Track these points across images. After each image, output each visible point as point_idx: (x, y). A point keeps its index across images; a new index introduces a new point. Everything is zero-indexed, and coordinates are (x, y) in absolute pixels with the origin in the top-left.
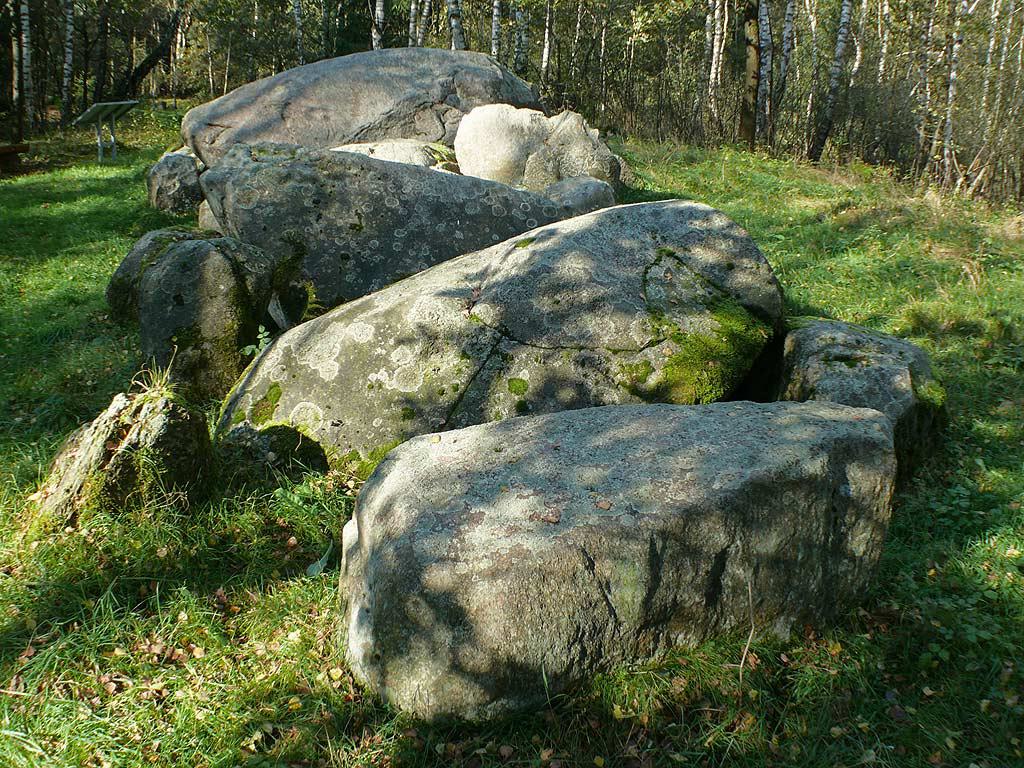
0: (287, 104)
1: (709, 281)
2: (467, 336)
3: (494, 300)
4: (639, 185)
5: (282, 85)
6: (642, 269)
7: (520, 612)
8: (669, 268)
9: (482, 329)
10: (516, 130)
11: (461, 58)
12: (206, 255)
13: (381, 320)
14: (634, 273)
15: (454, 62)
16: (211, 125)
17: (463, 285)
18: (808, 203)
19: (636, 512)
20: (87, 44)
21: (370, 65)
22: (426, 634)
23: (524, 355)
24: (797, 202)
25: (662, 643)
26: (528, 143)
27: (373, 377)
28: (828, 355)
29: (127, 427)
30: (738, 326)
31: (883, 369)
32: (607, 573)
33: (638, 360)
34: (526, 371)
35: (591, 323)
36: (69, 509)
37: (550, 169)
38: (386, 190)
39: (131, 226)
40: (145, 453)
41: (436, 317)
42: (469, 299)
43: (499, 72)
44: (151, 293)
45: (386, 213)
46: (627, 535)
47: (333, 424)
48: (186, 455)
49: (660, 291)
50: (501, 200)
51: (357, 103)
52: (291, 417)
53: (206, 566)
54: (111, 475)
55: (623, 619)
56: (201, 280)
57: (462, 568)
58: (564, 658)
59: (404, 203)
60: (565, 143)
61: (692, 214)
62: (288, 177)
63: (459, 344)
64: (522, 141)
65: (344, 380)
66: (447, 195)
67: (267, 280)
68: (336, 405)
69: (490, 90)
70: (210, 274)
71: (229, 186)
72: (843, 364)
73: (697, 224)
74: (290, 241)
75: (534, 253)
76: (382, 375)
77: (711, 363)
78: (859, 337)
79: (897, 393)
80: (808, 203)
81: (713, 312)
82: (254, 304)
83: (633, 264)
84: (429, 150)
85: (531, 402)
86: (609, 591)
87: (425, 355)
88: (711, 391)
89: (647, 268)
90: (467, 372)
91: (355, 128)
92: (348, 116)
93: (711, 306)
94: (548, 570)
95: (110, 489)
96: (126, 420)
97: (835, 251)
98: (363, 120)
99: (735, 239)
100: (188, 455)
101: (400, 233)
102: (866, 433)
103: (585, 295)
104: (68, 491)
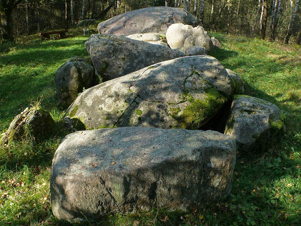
0: (125, 22)
1: (208, 82)
2: (127, 96)
3: (137, 86)
4: (223, 48)
5: (125, 16)
6: (185, 77)
7: (79, 194)
8: (195, 78)
9: (132, 94)
10: (183, 31)
11: (175, 10)
12: (71, 67)
13: (105, 89)
14: (182, 79)
15: (173, 11)
16: (104, 27)
17: (131, 80)
18: (272, 56)
19: (122, 167)
20: (89, 4)
21: (149, 12)
22: (58, 195)
23: (142, 103)
24: (269, 55)
25: (134, 208)
26: (187, 35)
27: (100, 106)
28: (242, 109)
29: (24, 118)
30: (214, 98)
31: (260, 116)
32: (110, 186)
33: (176, 107)
34: (143, 108)
35: (164, 95)
36: (6, 139)
37: (191, 43)
38: (133, 48)
39: (81, 54)
40: (27, 125)
41: (119, 90)
42: (131, 84)
43: (186, 14)
44: (57, 76)
45: (133, 55)
46: (118, 175)
47: (89, 119)
48: (40, 126)
49: (190, 85)
50: (167, 52)
51: (145, 21)
52: (79, 115)
53: (39, 158)
54: (17, 131)
55: (117, 200)
56: (70, 74)
57: (66, 178)
58: (95, 210)
59: (138, 52)
60: (197, 35)
61: (207, 60)
62: (106, 44)
63: (125, 98)
64: (185, 34)
65: (93, 106)
66: (151, 50)
67: (88, 74)
68: (90, 114)
69: (183, 19)
70: (72, 72)
71: (91, 46)
72: (247, 113)
73: (208, 64)
74: (105, 62)
75: (151, 71)
76: (102, 106)
77: (201, 110)
78: (255, 104)
79: (263, 124)
80: (272, 56)
81: (206, 92)
82: (84, 81)
83: (183, 76)
84: (159, 36)
85: (142, 118)
86: (111, 192)
87: (115, 101)
88: (199, 119)
89: (187, 77)
90: (126, 107)
91: (144, 29)
92: (142, 25)
93: (206, 90)
94: (88, 183)
95: (16, 134)
96: (24, 115)
97: (275, 71)
98: (146, 27)
99: (219, 69)
100: (41, 126)
101: (136, 61)
102: (220, 145)
103: (163, 86)
104: (6, 134)
